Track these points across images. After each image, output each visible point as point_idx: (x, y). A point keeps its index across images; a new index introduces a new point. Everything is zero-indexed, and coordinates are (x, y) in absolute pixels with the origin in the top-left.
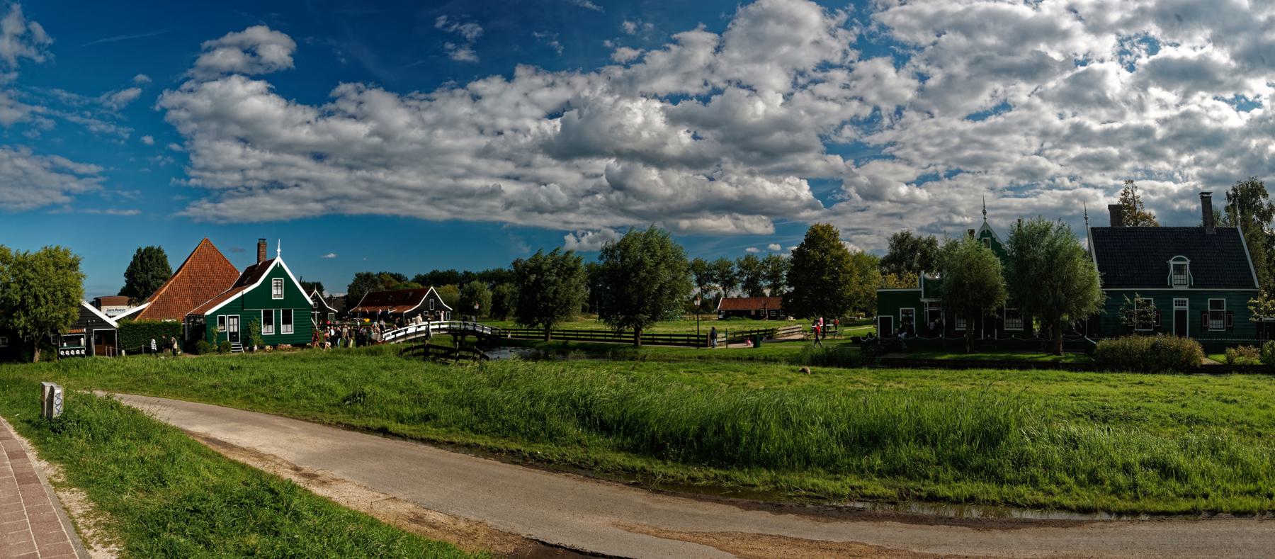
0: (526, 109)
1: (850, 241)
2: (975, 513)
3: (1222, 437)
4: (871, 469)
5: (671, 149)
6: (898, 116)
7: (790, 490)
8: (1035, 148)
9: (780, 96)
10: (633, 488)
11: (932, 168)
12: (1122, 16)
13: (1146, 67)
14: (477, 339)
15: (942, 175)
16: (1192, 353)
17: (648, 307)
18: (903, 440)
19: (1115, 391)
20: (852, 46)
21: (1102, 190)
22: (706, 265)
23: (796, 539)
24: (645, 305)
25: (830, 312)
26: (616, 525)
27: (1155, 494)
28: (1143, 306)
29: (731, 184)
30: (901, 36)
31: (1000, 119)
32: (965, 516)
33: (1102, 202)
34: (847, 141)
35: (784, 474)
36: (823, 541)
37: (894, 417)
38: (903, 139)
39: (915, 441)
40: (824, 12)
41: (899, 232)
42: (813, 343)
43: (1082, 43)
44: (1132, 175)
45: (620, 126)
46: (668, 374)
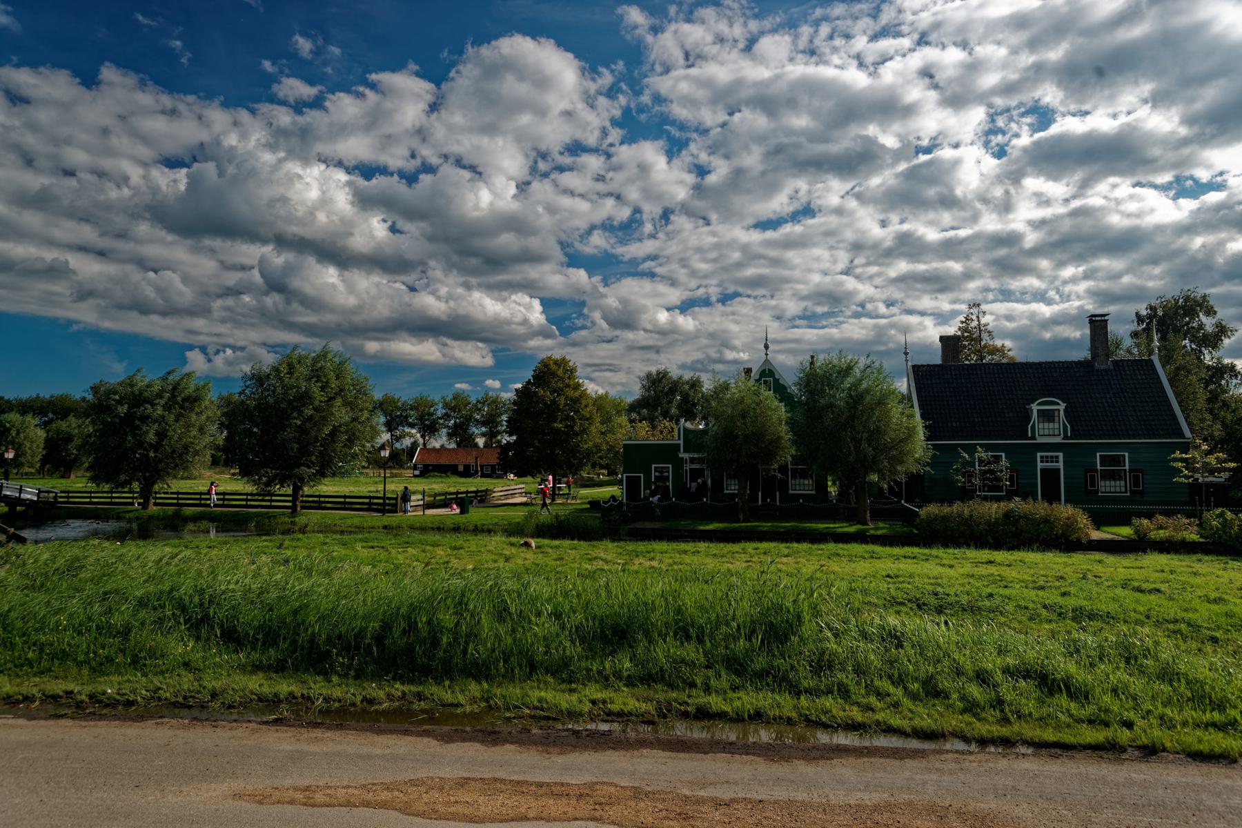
0: (120, 141)
1: (591, 380)
2: (765, 736)
3: (1141, 640)
4: (618, 675)
5: (359, 243)
6: (663, 222)
7: (508, 709)
8: (841, 266)
9: (513, 184)
10: (273, 728)
11: (701, 291)
12: (1003, 78)
13: (1025, 150)
14: (6, 509)
15: (714, 299)
16: (1073, 524)
17: (313, 458)
18: (659, 635)
19: (952, 572)
20: (615, 123)
21: (932, 317)
22: (400, 404)
23: (518, 782)
24: (312, 454)
25: (561, 468)
26: (237, 796)
27: (1036, 715)
28: (989, 463)
29: (439, 298)
30: (680, 112)
31: (798, 229)
32: (751, 739)
33: (931, 333)
34: (595, 251)
35: (499, 685)
36: (556, 783)
37: (646, 604)
38: (668, 252)
39: (675, 636)
40: (583, 70)
41: (654, 369)
42: (538, 508)
43: (932, 120)
44: (980, 297)
45: (284, 200)
46: (338, 551)
